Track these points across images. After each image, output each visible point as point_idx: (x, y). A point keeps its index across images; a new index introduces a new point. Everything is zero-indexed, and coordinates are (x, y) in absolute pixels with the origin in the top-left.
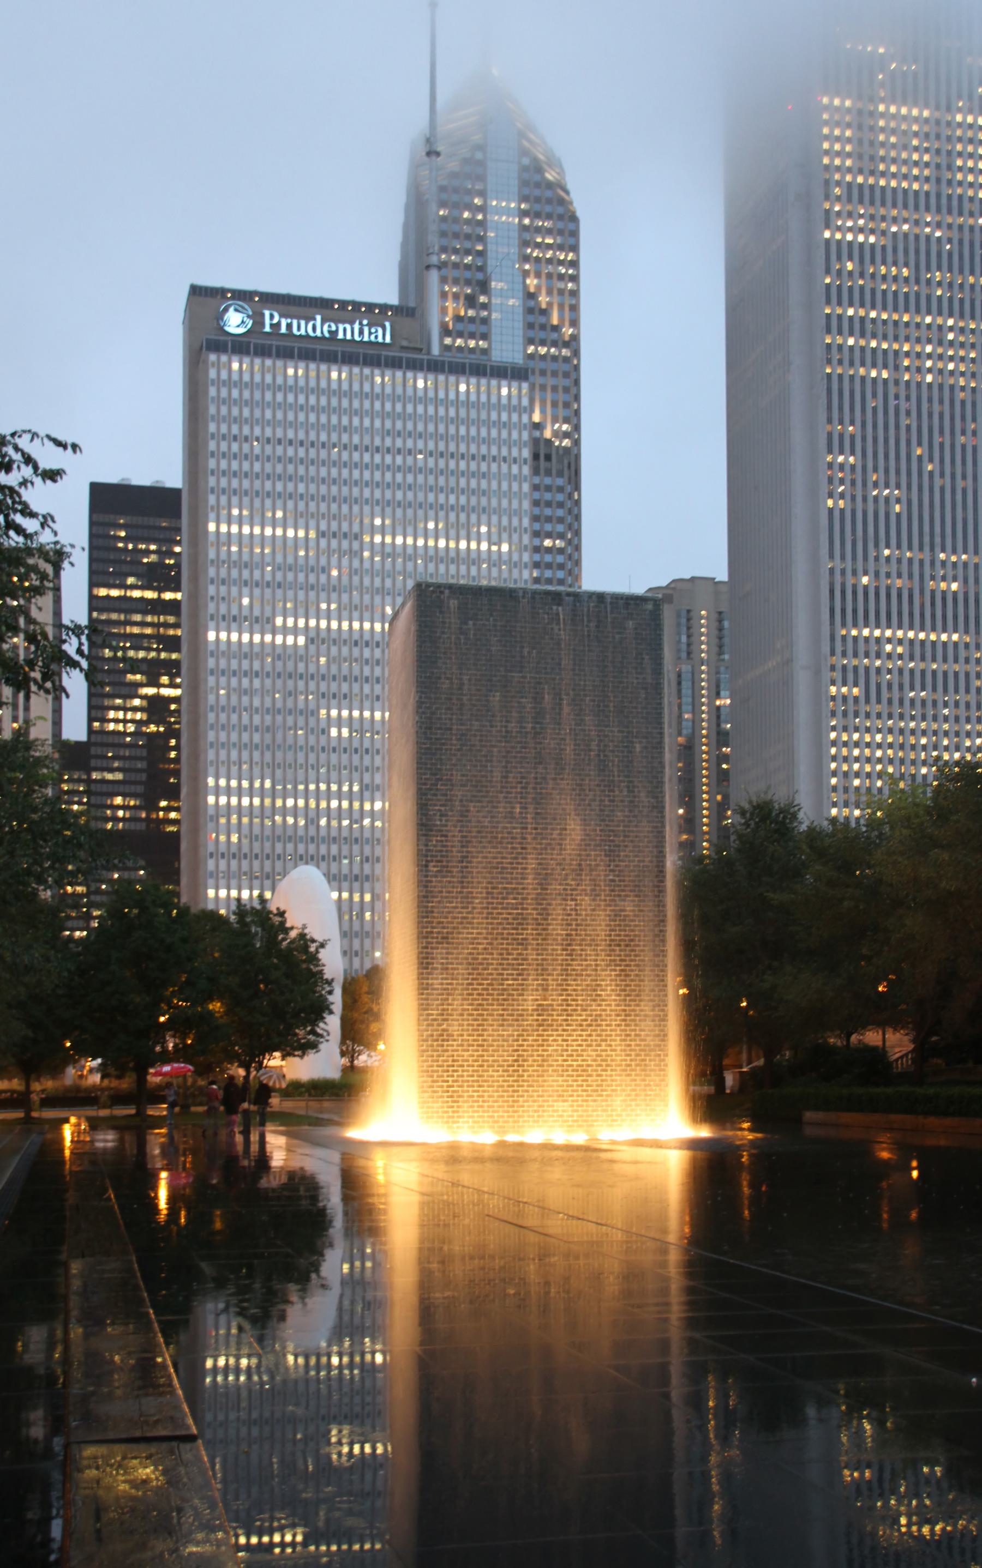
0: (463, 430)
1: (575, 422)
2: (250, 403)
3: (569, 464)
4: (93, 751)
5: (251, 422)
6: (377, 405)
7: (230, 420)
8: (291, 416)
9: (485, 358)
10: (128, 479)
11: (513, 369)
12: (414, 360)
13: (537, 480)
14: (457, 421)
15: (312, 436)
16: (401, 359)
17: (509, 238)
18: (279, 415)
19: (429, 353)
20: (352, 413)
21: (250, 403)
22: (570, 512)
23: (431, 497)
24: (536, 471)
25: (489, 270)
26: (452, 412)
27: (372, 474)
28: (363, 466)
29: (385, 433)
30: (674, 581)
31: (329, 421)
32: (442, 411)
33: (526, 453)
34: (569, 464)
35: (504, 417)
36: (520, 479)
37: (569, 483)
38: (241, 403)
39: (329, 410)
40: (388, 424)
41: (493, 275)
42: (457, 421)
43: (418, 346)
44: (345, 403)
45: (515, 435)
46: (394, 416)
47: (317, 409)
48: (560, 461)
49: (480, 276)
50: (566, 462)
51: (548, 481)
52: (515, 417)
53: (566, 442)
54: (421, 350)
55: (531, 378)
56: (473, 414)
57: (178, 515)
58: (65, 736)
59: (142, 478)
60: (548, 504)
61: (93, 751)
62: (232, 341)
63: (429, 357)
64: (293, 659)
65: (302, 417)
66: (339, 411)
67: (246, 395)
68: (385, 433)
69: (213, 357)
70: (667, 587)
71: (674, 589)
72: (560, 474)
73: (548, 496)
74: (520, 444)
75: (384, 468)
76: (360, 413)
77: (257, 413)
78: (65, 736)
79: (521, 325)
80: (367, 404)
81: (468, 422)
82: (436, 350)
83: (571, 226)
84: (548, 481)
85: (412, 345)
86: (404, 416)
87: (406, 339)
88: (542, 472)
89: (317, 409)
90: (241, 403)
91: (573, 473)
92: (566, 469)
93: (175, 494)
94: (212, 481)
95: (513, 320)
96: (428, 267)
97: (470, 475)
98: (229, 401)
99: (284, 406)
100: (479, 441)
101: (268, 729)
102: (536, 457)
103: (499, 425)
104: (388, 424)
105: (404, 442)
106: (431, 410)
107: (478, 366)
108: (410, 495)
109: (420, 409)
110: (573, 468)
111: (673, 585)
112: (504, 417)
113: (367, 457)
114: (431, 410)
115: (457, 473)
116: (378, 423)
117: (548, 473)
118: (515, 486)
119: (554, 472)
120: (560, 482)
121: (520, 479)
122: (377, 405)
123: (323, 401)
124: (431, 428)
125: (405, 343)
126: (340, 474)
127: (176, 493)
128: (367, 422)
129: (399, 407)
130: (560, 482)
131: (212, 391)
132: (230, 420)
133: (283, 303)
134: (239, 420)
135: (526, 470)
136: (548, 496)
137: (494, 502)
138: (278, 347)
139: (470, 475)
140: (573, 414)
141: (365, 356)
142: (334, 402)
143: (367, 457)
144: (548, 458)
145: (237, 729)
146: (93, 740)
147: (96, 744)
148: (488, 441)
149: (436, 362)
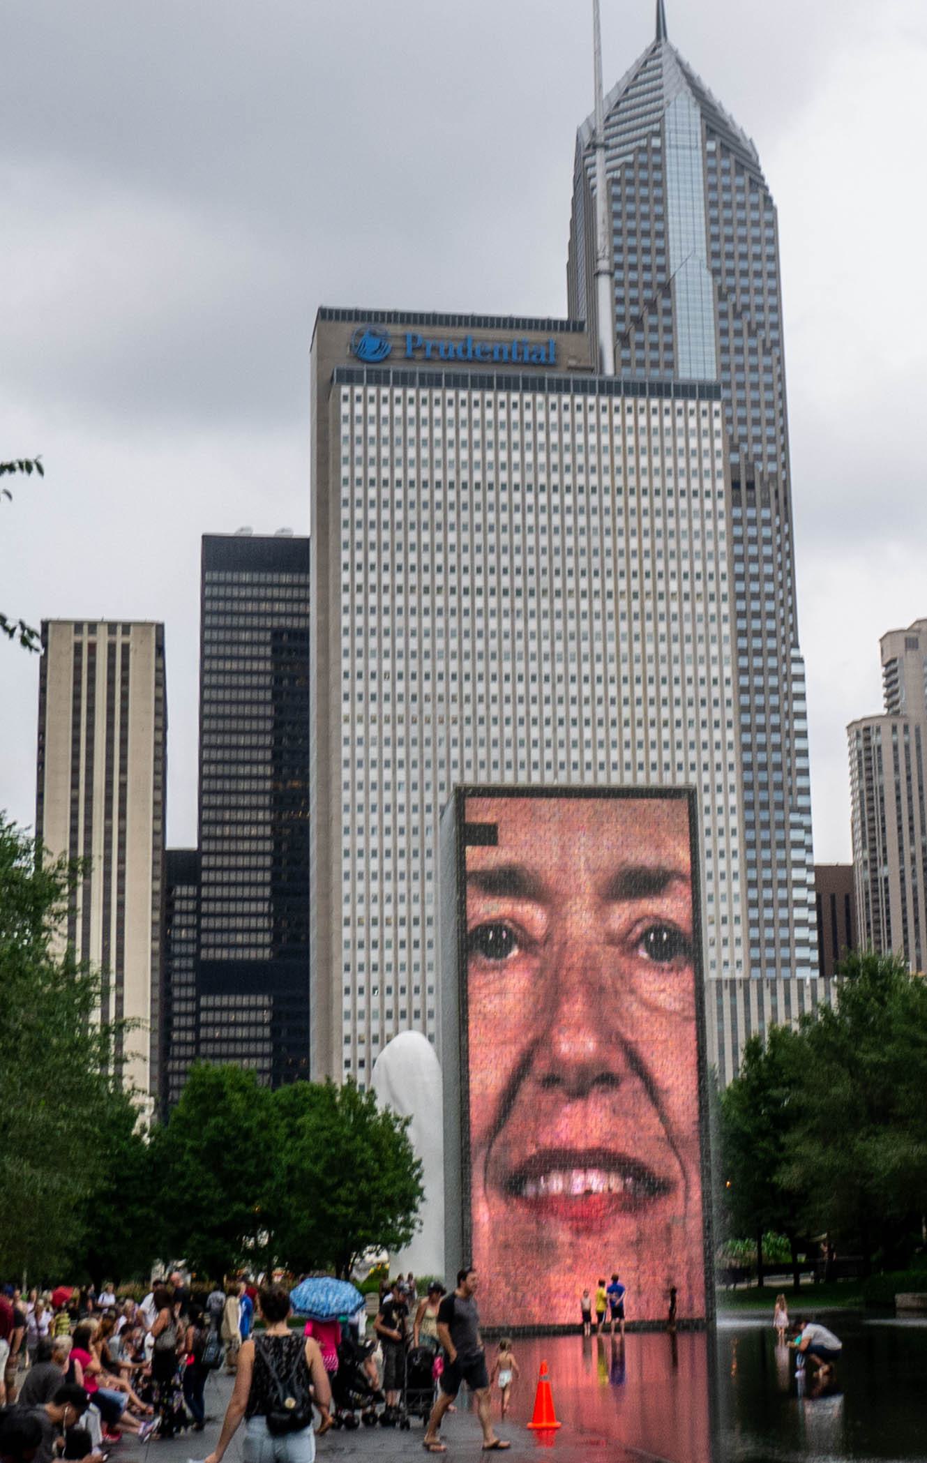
0: (644, 461)
1: (779, 370)
2: (391, 441)
5: (392, 463)
6: (541, 437)
7: (366, 462)
8: (438, 454)
9: (669, 373)
10: (249, 529)
11: (702, 387)
12: (584, 382)
13: (737, 512)
14: (637, 451)
15: (464, 475)
16: (568, 381)
18: (425, 453)
19: (602, 371)
20: (510, 446)
21: (391, 441)
22: (780, 566)
23: (608, 542)
24: (736, 502)
25: (672, 271)
26: (631, 441)
27: (537, 517)
28: (524, 509)
29: (551, 468)
30: (918, 622)
31: (484, 457)
32: (618, 440)
33: (721, 485)
35: (693, 443)
36: (715, 515)
37: (778, 513)
38: (379, 441)
39: (483, 445)
40: (555, 458)
41: (677, 278)
42: (637, 451)
43: (589, 364)
44: (503, 436)
45: (707, 464)
46: (561, 448)
47: (470, 445)
48: (765, 489)
49: (661, 277)
50: (772, 490)
51: (751, 513)
52: (706, 443)
53: (772, 467)
54: (591, 370)
56: (656, 441)
57: (305, 569)
59: (265, 527)
60: (763, 767)
63: (602, 378)
64: (444, 744)
65: (451, 454)
66: (496, 445)
67: (385, 431)
68: (551, 468)
69: (345, 390)
70: (909, 630)
71: (919, 631)
72: (766, 504)
73: (765, 835)
74: (714, 475)
75: (550, 510)
76: (522, 446)
77: (399, 452)
80: (529, 436)
81: (650, 451)
82: (609, 370)
83: (768, 216)
84: (751, 513)
85: (582, 364)
86: (573, 448)
87: (574, 357)
88: (744, 502)
89: (470, 445)
90: (379, 441)
93: (301, 545)
94: (345, 513)
95: (693, 216)
96: (598, 274)
97: (654, 513)
98: (365, 440)
99: (431, 443)
100: (664, 472)
101: (415, 831)
102: (735, 485)
103: (688, 453)
104: (555, 458)
105: (574, 478)
106: (605, 439)
107: (660, 386)
108: (583, 541)
109: (593, 439)
111: (917, 627)
112: (693, 443)
113: (530, 498)
114: (605, 439)
115: (640, 513)
116: (542, 458)
117: (751, 503)
118: (709, 525)
119: (758, 502)
120: (766, 514)
121: (715, 515)
122: (541, 437)
123: (477, 434)
124: (606, 460)
125: (573, 363)
126: (498, 519)
127: (305, 542)
128: (529, 457)
129: (567, 438)
130: (766, 514)
131: (345, 430)
132: (366, 462)
133: (428, 323)
134: (378, 462)
135: (721, 505)
136: (765, 835)
137: (685, 545)
138: (422, 375)
139: (654, 513)
140: (775, 362)
141: (525, 380)
142: (490, 435)
143: (530, 498)
144: (750, 486)
145: (378, 832)
146: (205, 847)
147: (208, 853)
148: (675, 473)
149: (610, 383)
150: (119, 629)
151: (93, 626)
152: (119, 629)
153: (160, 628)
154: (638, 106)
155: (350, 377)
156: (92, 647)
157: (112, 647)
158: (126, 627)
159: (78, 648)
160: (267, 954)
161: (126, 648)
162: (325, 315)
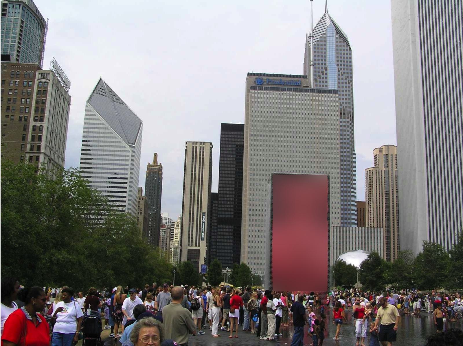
3: (350, 115)
4: (219, 196)
13: (341, 120)
17: (330, 52)
34: (350, 115)
37: (351, 120)
50: (349, 115)
51: (344, 120)
55: (339, 93)
58: (212, 192)
61: (219, 196)
62: (6, 9)
72: (348, 118)
78: (212, 192)
79: (327, 57)
84: (344, 120)
88: (343, 118)
91: (351, 118)
92: (349, 117)
96: (311, 65)
102: (341, 114)
110: (351, 116)
117: (344, 118)
120: (348, 120)
125: (305, 85)
130: (348, 120)
135: (338, 118)
136: (346, 221)
147: (221, 194)
150: (202, 143)
151: (197, 143)
152: (202, 143)
153: (211, 144)
154: (105, 160)
155: (254, 88)
156: (196, 147)
157: (200, 148)
158: (204, 143)
159: (193, 147)
160: (232, 216)
161: (203, 147)
162: (249, 74)
